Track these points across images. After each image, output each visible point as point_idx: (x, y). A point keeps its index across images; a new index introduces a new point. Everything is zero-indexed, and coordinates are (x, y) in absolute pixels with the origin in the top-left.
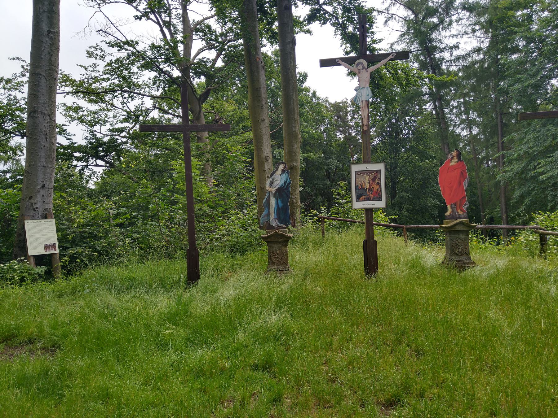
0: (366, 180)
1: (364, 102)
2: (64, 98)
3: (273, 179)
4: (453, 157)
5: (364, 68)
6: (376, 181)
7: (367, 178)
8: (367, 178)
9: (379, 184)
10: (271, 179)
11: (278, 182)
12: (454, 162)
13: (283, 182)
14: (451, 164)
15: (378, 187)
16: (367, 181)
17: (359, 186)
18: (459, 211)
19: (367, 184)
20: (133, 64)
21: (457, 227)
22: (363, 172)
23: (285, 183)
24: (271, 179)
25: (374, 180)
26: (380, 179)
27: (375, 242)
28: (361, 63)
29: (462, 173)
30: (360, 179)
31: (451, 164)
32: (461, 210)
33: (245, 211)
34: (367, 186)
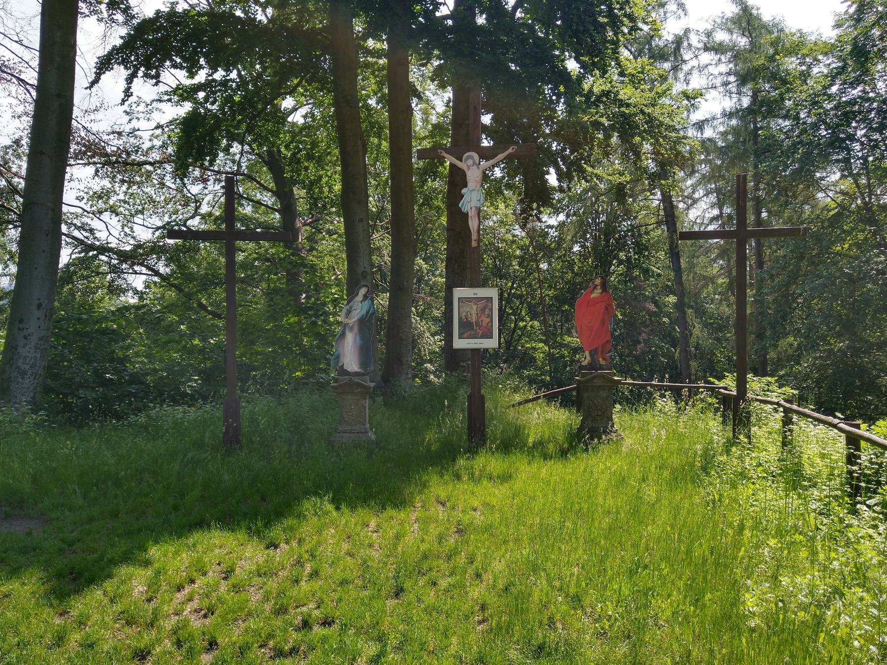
0: (473, 310)
1: (473, 209)
2: (80, 180)
3: (351, 308)
4: (596, 285)
5: (474, 163)
6: (486, 313)
7: (475, 307)
8: (475, 307)
9: (490, 316)
10: (348, 307)
11: (358, 311)
12: (597, 293)
13: (364, 311)
14: (593, 296)
15: (488, 320)
16: (474, 312)
17: (464, 317)
18: (601, 359)
19: (474, 316)
20: (732, 523)
21: (595, 381)
22: (469, 300)
23: (368, 312)
24: (348, 307)
25: (483, 310)
26: (491, 310)
27: (482, 398)
28: (471, 157)
29: (607, 308)
30: (466, 309)
31: (593, 296)
32: (604, 359)
33: (416, 526)
34: (474, 319)
